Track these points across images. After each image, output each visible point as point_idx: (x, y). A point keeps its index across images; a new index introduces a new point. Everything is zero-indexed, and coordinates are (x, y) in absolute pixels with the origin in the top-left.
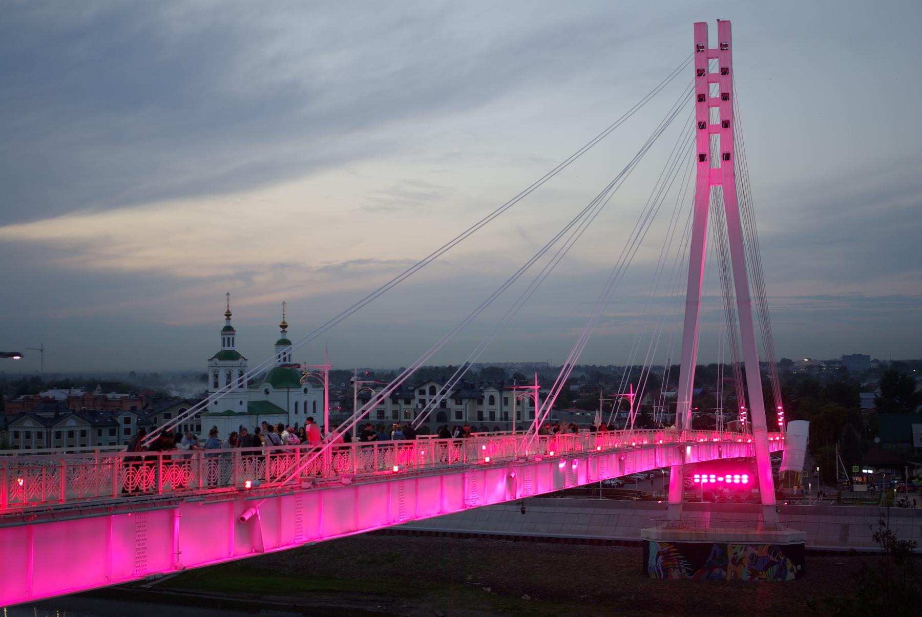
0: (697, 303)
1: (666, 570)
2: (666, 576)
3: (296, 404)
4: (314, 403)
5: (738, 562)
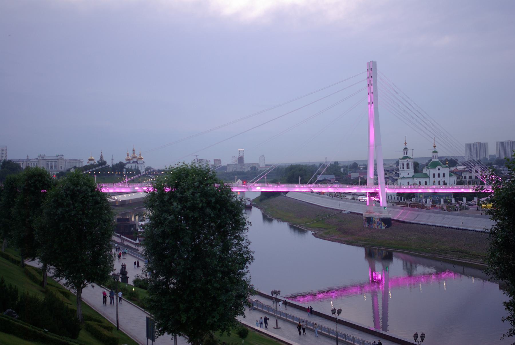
4: (444, 174)
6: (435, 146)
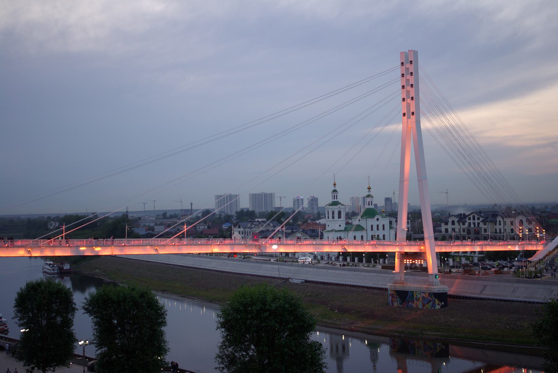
0: (403, 182)
1: (392, 302)
2: (393, 305)
3: (372, 226)
4: (383, 226)
5: (418, 300)
6: (369, 189)
